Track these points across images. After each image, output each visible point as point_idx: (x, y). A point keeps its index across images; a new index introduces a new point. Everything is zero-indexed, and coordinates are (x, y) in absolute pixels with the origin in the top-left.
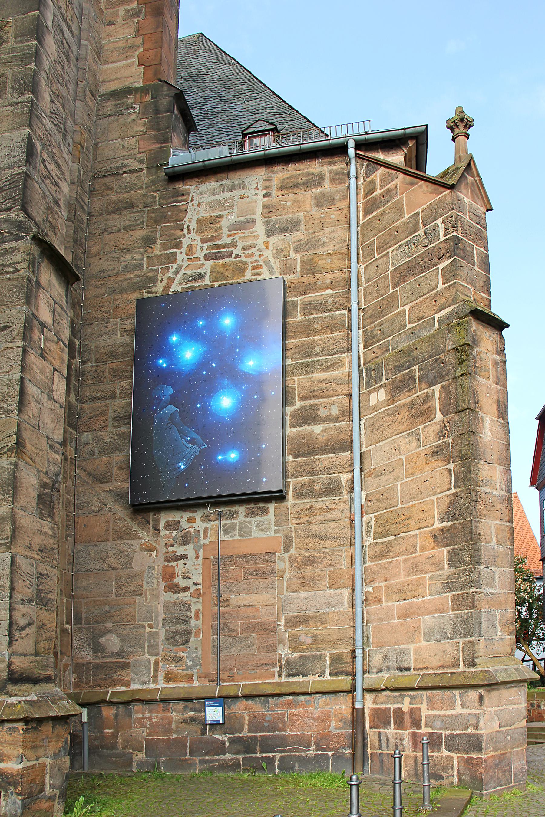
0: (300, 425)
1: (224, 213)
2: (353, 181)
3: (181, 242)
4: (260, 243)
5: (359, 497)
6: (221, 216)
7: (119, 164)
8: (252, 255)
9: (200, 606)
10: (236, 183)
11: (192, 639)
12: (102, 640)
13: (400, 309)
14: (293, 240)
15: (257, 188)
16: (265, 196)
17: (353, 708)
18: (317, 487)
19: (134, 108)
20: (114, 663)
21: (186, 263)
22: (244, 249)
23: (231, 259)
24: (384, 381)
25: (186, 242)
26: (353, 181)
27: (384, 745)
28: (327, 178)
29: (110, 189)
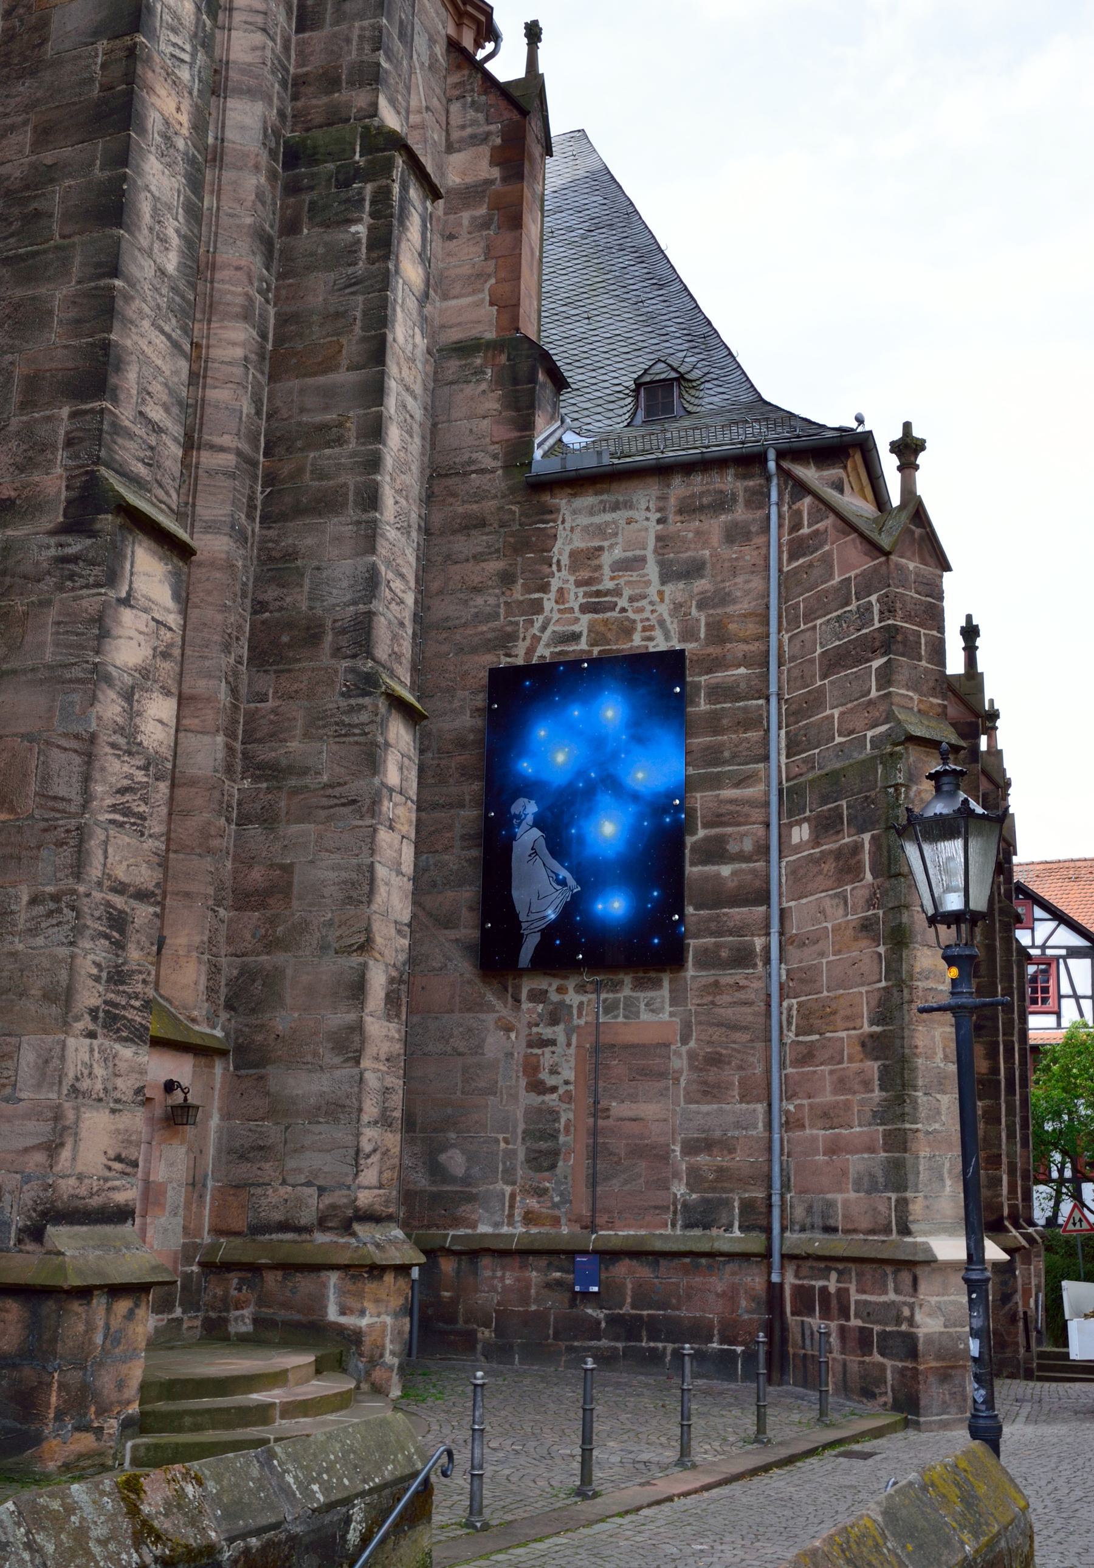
0: (704, 863)
1: (606, 544)
2: (774, 510)
3: (548, 584)
4: (653, 591)
5: (778, 972)
6: (601, 549)
7: (466, 457)
8: (641, 610)
9: (571, 1116)
10: (621, 499)
11: (560, 1164)
12: (443, 1158)
13: (828, 712)
14: (696, 591)
15: (648, 509)
16: (659, 521)
17: (769, 1282)
18: (724, 954)
19: (485, 373)
20: (456, 1192)
21: (556, 616)
22: (632, 599)
23: (615, 614)
24: (808, 814)
25: (555, 584)
26: (774, 510)
27: (808, 1342)
28: (741, 499)
29: (454, 495)
